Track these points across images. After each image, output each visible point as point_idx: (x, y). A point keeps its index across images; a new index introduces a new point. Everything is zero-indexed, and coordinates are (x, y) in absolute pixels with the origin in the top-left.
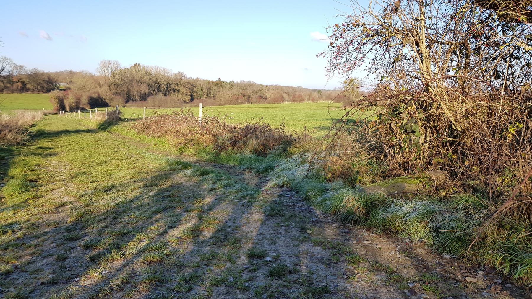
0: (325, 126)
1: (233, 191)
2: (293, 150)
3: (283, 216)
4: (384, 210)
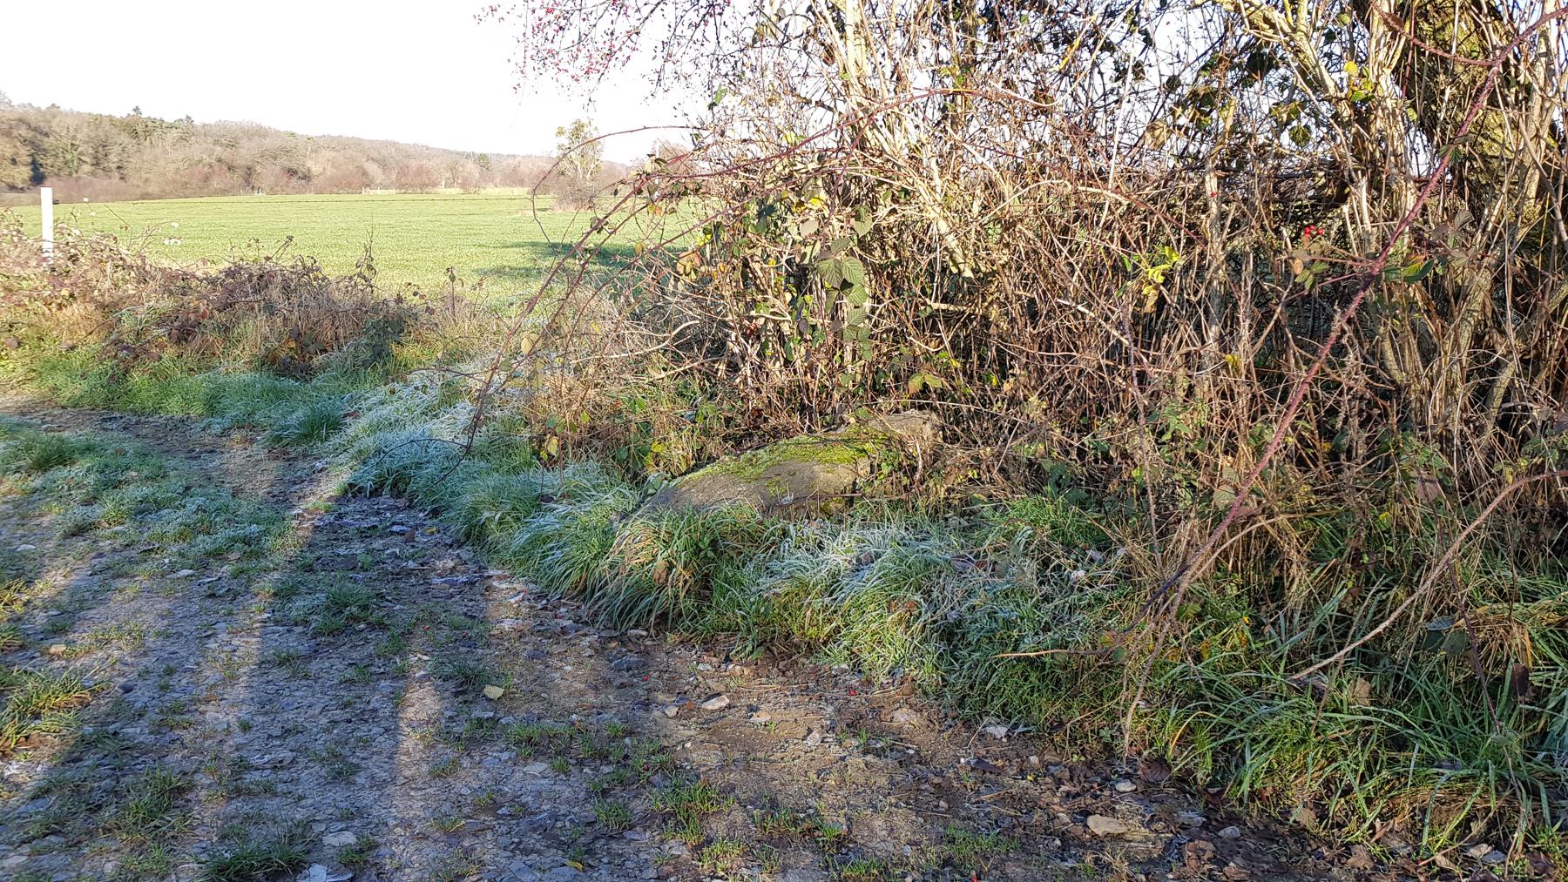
0: (514, 264)
1: (171, 529)
2: (409, 351)
3: (381, 626)
4: (757, 568)
